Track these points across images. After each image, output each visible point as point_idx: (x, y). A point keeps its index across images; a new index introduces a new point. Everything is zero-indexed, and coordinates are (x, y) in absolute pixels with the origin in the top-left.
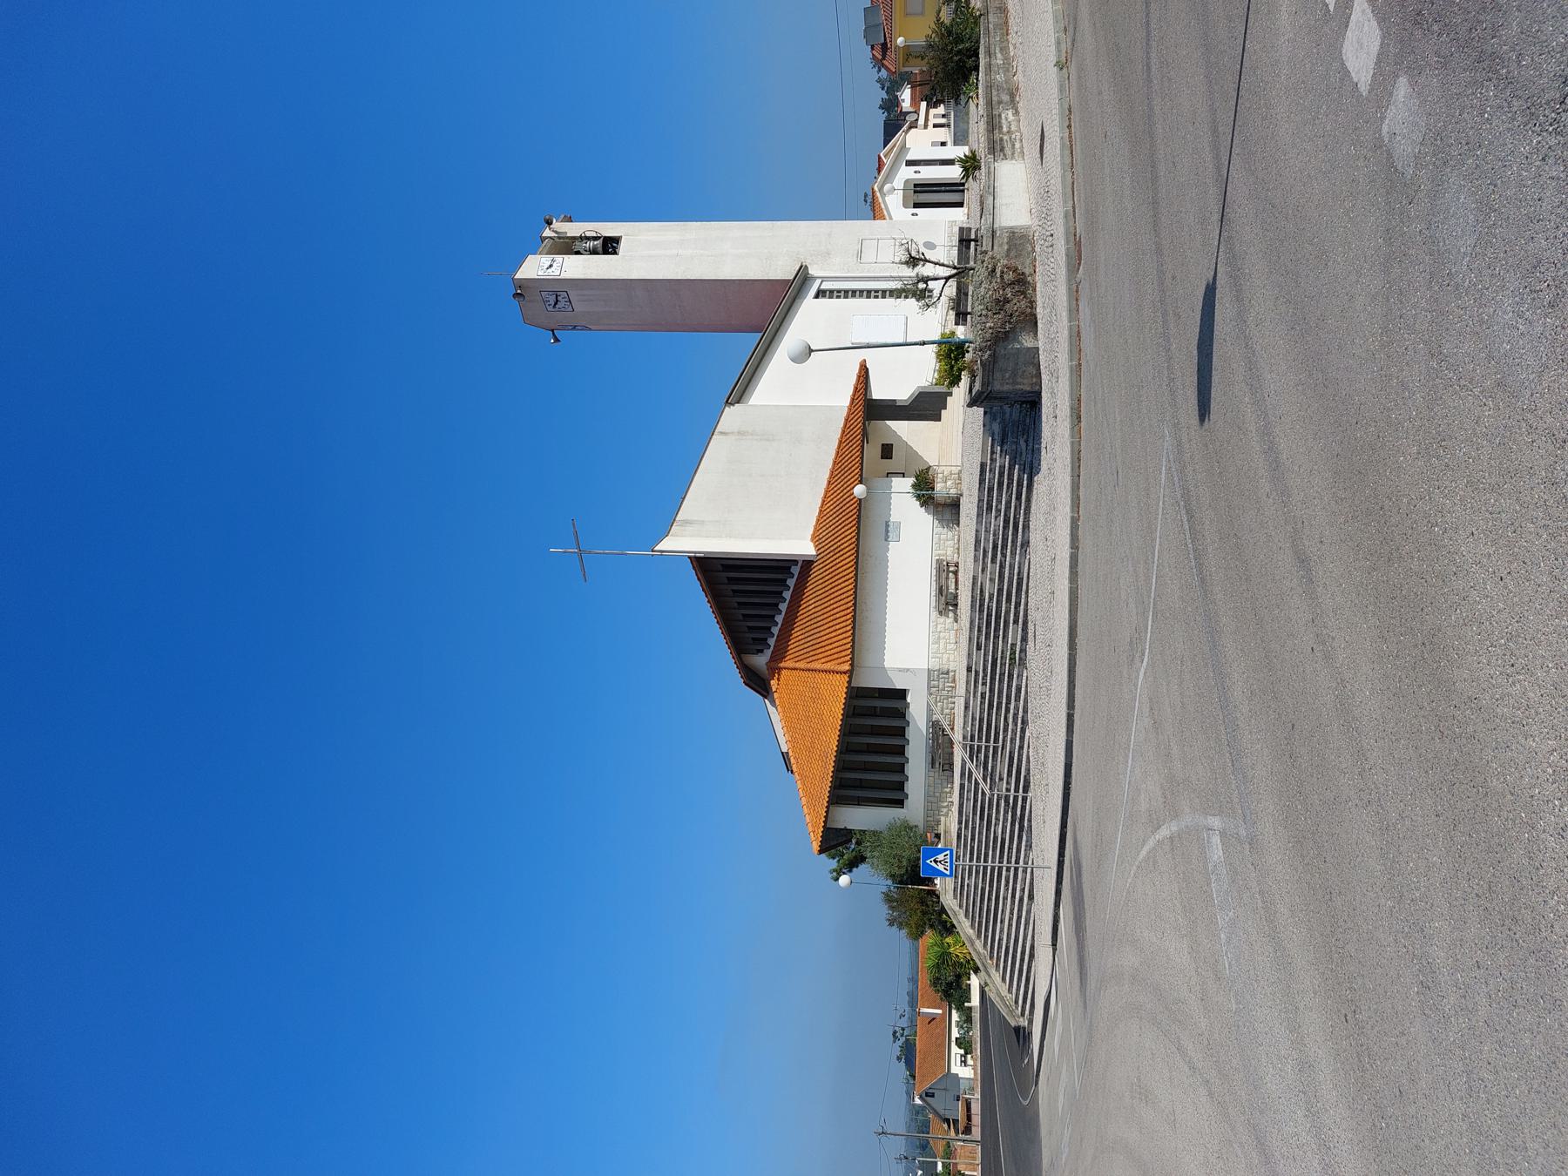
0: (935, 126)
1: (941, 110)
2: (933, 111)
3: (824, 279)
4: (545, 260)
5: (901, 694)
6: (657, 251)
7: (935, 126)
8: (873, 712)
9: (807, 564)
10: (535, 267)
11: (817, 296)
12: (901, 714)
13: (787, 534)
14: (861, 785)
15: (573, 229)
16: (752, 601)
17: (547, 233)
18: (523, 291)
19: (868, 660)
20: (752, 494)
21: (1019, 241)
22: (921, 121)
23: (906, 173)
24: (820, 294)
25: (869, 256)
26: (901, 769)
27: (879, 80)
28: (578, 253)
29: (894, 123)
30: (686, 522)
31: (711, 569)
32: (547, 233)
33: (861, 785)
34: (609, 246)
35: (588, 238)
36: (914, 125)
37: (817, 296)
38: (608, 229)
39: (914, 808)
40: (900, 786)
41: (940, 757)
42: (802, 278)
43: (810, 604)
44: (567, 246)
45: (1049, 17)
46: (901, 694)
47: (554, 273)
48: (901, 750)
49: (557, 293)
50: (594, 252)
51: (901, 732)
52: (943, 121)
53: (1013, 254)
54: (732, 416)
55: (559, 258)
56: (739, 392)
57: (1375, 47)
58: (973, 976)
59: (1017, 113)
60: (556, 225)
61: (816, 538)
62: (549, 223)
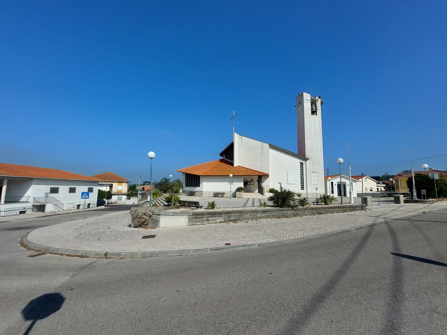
0: (378, 189)
1: (383, 189)
2: (383, 188)
3: (306, 164)
6: (313, 126)
7: (378, 189)
9: (232, 164)
10: (307, 97)
11: (301, 163)
13: (239, 160)
15: (319, 104)
16: (228, 154)
17: (317, 98)
19: (204, 179)
20: (248, 152)
21: (156, 223)
22: (378, 185)
23: (348, 182)
24: (302, 164)
25: (313, 174)
28: (312, 106)
30: (242, 138)
31: (231, 147)
32: (317, 98)
34: (314, 112)
35: (316, 107)
36: (377, 183)
37: (301, 163)
38: (319, 112)
42: (306, 159)
44: (313, 103)
45: (168, 248)
47: (305, 101)
49: (301, 103)
50: (312, 109)
52: (379, 190)
53: (153, 221)
54: (266, 146)
55: (310, 102)
56: (272, 146)
59: (221, 222)
60: (320, 100)
62: (319, 98)
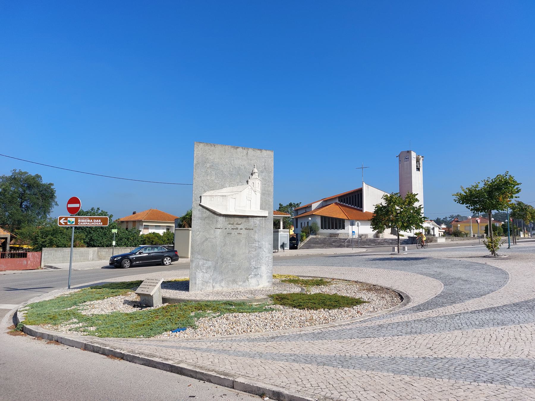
4: (415, 157)
5: (344, 228)
8: (340, 224)
9: (362, 211)
10: (414, 155)
12: (340, 228)
14: (325, 221)
15: (421, 162)
18: (409, 152)
26: (329, 228)
27: (446, 218)
29: (439, 222)
33: (325, 221)
34: (418, 169)
38: (421, 169)
39: (322, 231)
40: (325, 228)
41: (331, 235)
43: (355, 211)
44: (418, 161)
46: (344, 228)
47: (413, 159)
48: (333, 228)
49: (409, 159)
51: (336, 228)
57: (408, 354)
58: (141, 233)
61: (366, 212)
